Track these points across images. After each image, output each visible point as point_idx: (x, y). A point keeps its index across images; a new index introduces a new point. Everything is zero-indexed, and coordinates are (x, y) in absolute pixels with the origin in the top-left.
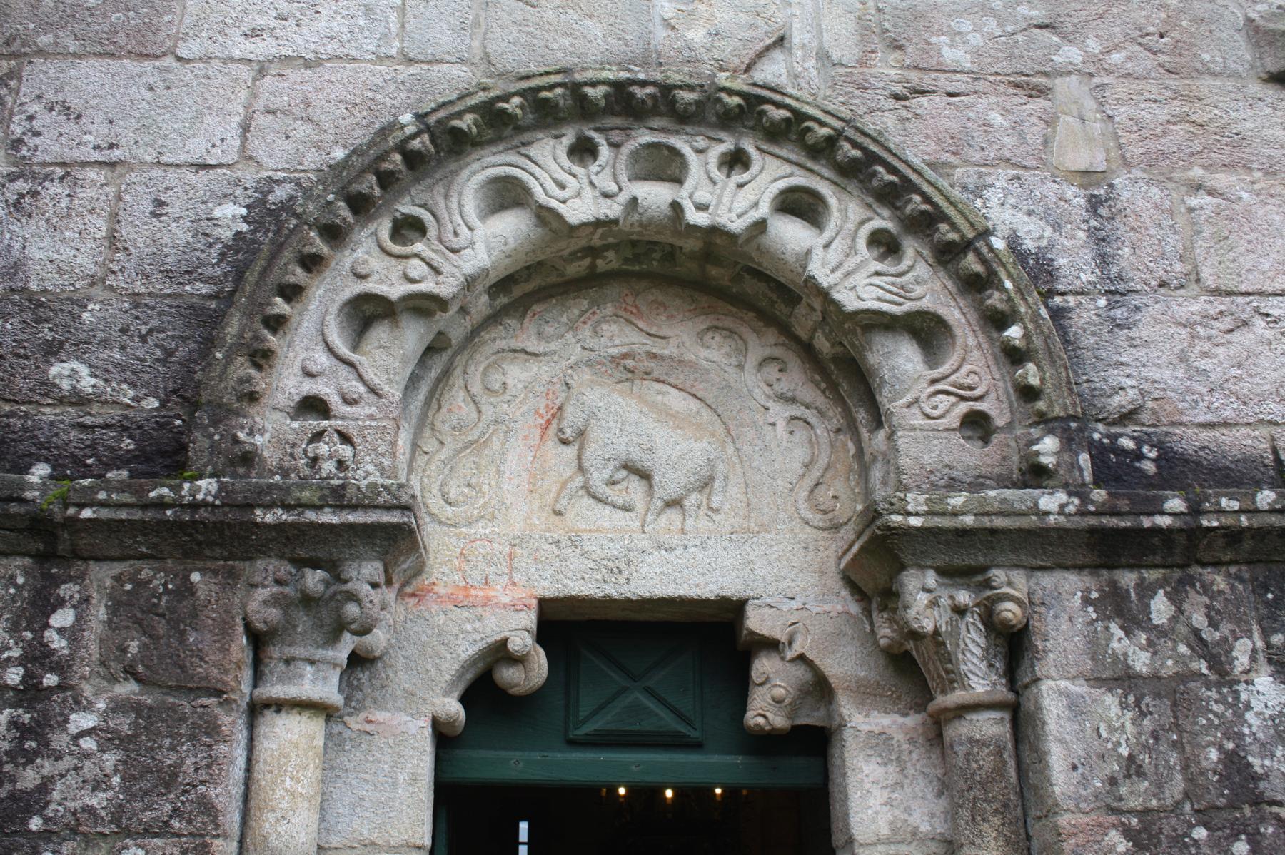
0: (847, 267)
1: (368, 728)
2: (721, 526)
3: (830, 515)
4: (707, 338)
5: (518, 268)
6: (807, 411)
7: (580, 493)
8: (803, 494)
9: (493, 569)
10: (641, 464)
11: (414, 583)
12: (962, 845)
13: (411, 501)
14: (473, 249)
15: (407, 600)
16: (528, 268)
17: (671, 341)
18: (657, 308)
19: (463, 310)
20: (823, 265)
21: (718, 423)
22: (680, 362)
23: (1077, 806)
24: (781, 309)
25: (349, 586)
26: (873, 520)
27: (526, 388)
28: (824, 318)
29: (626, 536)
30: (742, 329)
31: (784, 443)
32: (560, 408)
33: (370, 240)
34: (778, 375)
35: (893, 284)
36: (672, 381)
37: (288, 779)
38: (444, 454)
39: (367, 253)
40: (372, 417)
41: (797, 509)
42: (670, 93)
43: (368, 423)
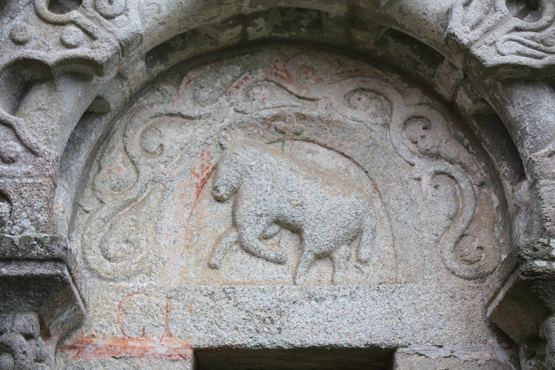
0: (486, 24)
2: (370, 277)
3: (476, 266)
4: (354, 99)
5: (173, 35)
6: (451, 166)
7: (235, 247)
8: (449, 245)
9: (150, 321)
10: (292, 219)
11: (74, 336)
13: (64, 253)
14: (127, 15)
15: (67, 352)
16: (183, 36)
17: (320, 103)
18: (306, 73)
19: (121, 76)
20: (463, 23)
21: (365, 180)
22: (328, 122)
24: (424, 70)
26: (517, 265)
27: (182, 149)
28: (466, 76)
29: (278, 287)
30: (387, 90)
31: (430, 197)
32: (215, 168)
33: (27, 8)
34: (423, 133)
35: (532, 39)
36: (321, 140)
38: (104, 212)
39: (26, 21)
40: (28, 175)
41: (443, 260)
43: (24, 180)
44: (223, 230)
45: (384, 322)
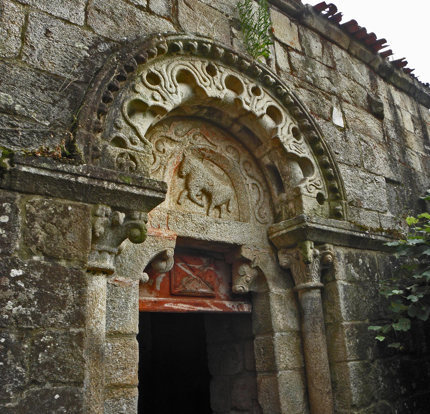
1: (116, 283)
12: (309, 332)
23: (347, 319)
25: (137, 222)
37: (100, 304)
42: (241, 60)
44: (182, 189)
45: (239, 235)
